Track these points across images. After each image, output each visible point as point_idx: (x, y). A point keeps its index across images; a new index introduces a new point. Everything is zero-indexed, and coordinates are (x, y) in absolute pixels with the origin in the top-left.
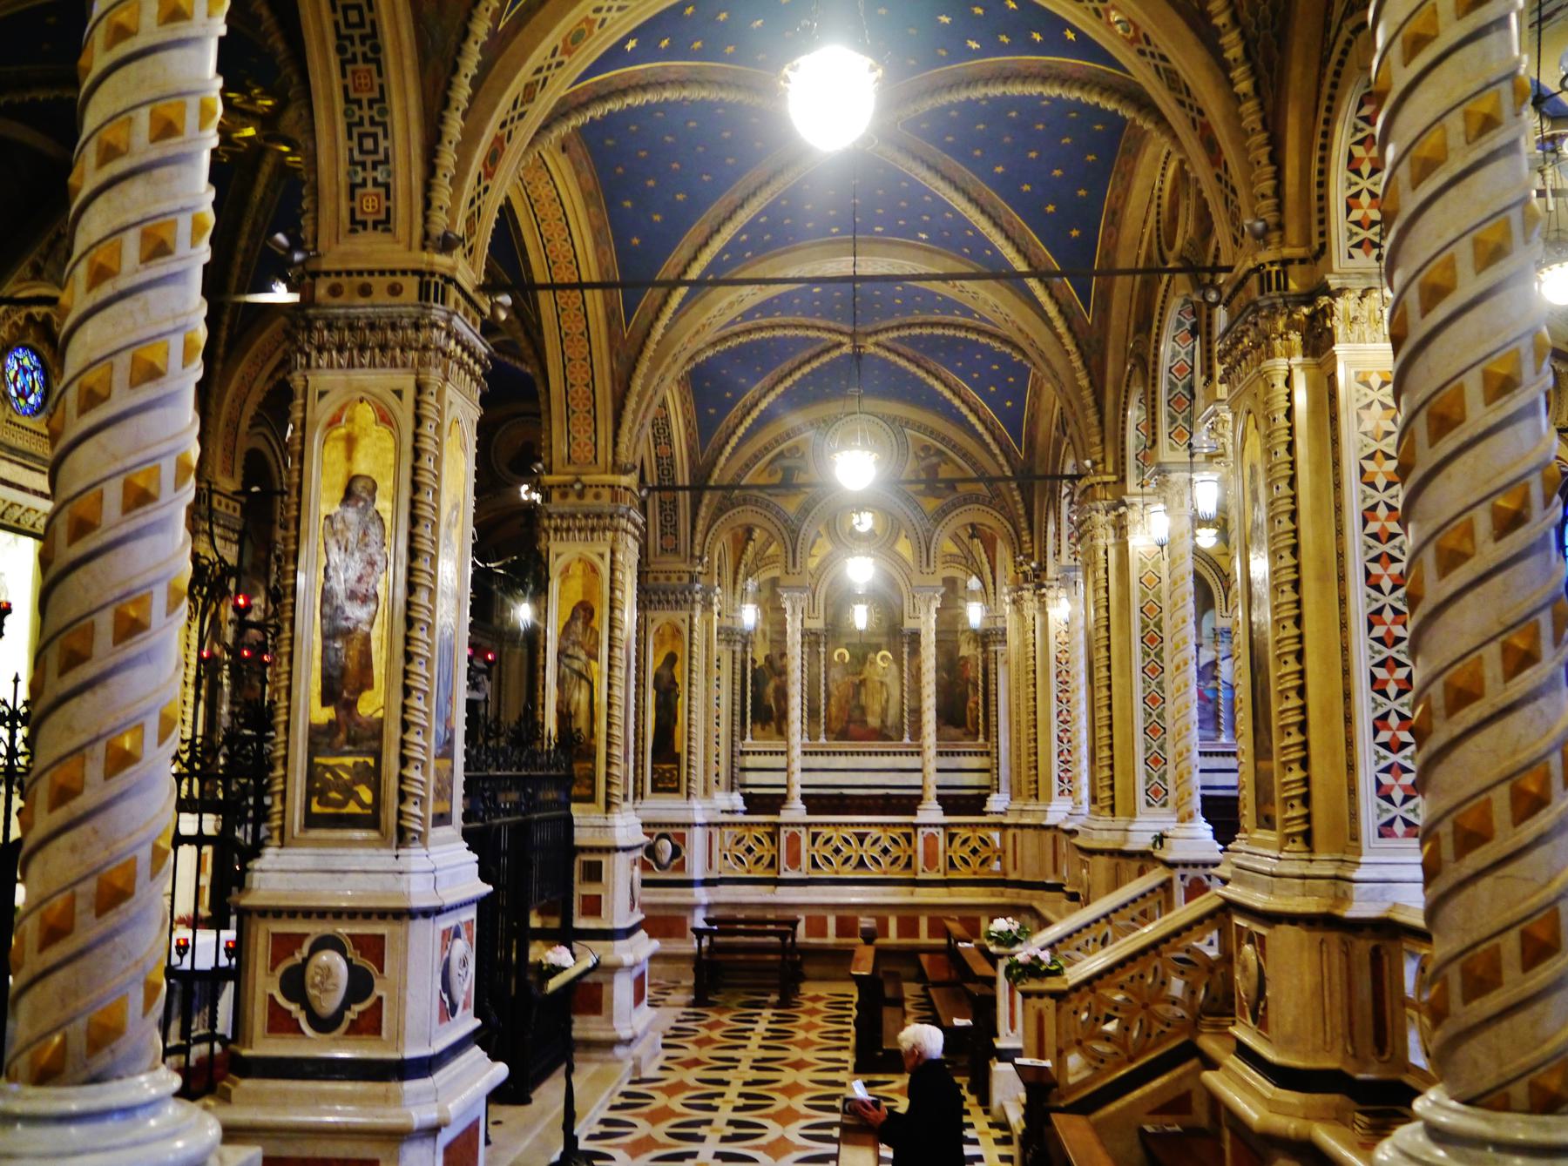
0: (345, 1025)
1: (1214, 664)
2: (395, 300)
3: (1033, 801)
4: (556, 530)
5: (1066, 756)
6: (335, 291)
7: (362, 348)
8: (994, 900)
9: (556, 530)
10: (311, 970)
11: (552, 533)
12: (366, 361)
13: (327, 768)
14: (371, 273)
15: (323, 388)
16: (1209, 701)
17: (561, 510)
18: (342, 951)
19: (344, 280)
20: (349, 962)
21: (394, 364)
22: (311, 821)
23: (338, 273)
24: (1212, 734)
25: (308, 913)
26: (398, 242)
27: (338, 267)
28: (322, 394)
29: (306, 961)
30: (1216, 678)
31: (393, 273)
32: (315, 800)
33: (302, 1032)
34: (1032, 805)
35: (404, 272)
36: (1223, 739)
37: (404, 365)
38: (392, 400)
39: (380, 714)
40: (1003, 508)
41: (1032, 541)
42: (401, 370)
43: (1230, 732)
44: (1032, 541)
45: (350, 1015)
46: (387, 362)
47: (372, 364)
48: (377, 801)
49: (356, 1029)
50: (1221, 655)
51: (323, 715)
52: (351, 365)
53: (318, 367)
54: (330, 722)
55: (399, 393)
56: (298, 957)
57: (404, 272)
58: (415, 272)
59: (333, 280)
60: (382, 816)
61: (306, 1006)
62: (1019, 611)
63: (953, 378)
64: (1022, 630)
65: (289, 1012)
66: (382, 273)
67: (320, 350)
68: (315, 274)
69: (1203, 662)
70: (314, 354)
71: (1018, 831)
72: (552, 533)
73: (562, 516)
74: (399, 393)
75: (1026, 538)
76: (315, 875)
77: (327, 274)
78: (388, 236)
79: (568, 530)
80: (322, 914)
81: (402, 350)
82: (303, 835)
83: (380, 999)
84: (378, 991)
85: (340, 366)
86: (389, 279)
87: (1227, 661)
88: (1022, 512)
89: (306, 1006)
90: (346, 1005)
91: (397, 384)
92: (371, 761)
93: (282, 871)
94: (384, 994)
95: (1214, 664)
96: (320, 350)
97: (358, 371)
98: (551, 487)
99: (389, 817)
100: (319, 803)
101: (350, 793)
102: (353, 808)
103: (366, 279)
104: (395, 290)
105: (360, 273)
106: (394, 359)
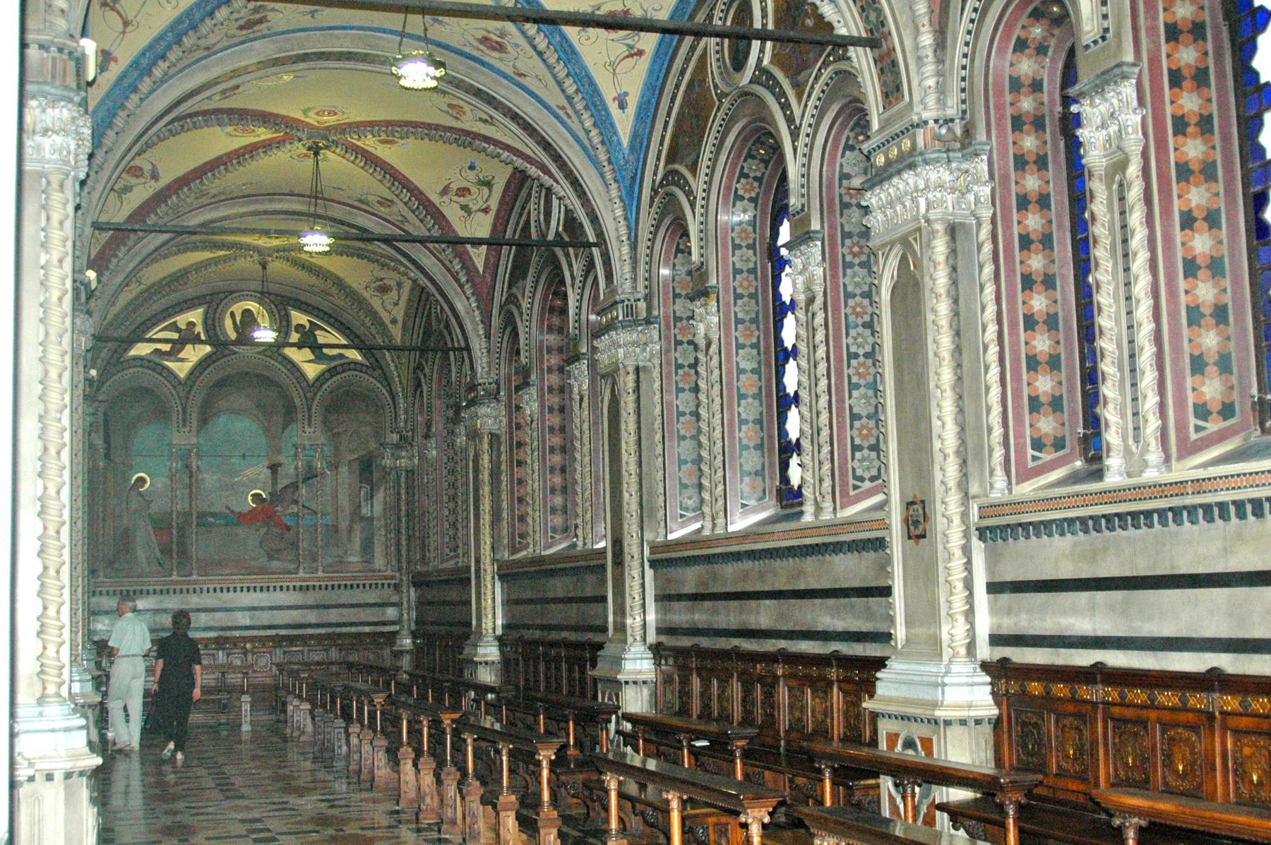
16: (288, 529)
36: (301, 574)
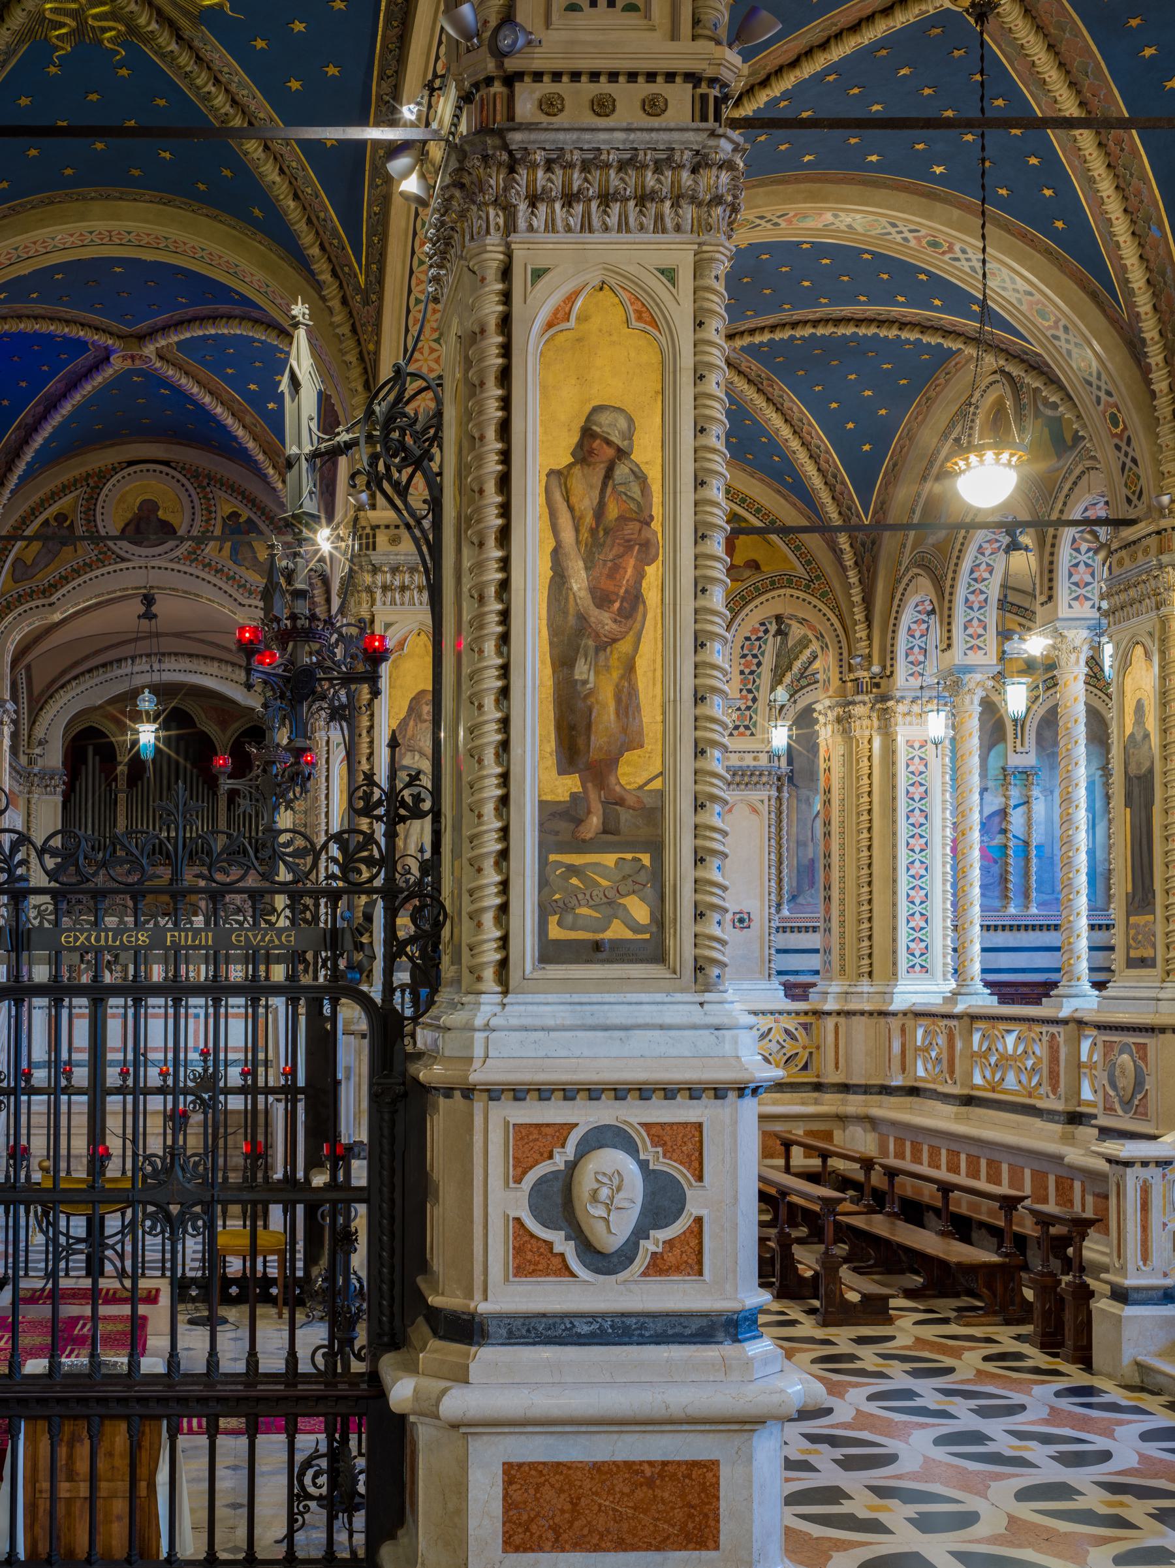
0: (640, 1263)
1: (1003, 813)
2: (655, 122)
3: (865, 980)
4: (385, 588)
5: (918, 921)
6: (550, 105)
7: (606, 199)
8: (810, 1109)
9: (385, 588)
10: (585, 1182)
11: (378, 594)
12: (613, 221)
13: (573, 870)
14: (613, 76)
15: (541, 264)
17: (393, 560)
18: (631, 1149)
19: (564, 87)
20: (643, 1165)
21: (659, 225)
22: (551, 953)
23: (557, 76)
24: (997, 903)
25: (569, 1093)
26: (653, 29)
27: (558, 65)
28: (538, 274)
29: (572, 1166)
30: (1004, 831)
31: (651, 77)
32: (553, 920)
33: (573, 1275)
34: (865, 986)
35: (670, 77)
36: (1012, 910)
37: (678, 228)
38: (658, 286)
39: (657, 784)
40: (824, 595)
41: (869, 637)
42: (672, 236)
43: (1021, 900)
44: (869, 637)
45: (648, 1246)
46: (649, 222)
47: (623, 226)
48: (659, 921)
49: (658, 1267)
50: (1012, 803)
51: (566, 786)
52: (586, 226)
53: (531, 228)
54: (573, 796)
55: (669, 274)
56: (559, 1161)
57: (670, 77)
58: (693, 78)
59: (547, 87)
60: (670, 942)
61: (578, 1234)
62: (846, 733)
63: (797, 407)
64: (850, 758)
65: (550, 1245)
66: (632, 76)
67: (533, 200)
68: (511, 80)
69: (988, 811)
70: (523, 207)
71: (842, 1020)
72: (379, 592)
73: (395, 570)
74: (669, 274)
75: (861, 633)
76: (580, 1034)
77: (538, 76)
78: (632, 19)
79: (403, 588)
80: (593, 1093)
81: (676, 205)
82: (538, 974)
83: (699, 1220)
84: (693, 1208)
85: (569, 229)
86: (643, 89)
87: (1020, 810)
88: (857, 599)
89: (578, 1234)
90: (640, 1232)
91: (667, 261)
92: (646, 859)
93: (526, 1029)
94: (704, 1212)
95: (1003, 813)
96: (533, 200)
97: (598, 236)
98: (375, 528)
99: (683, 948)
100: (559, 924)
101: (611, 907)
102: (617, 931)
103: (604, 87)
104: (653, 106)
105: (595, 76)
106: (659, 217)
